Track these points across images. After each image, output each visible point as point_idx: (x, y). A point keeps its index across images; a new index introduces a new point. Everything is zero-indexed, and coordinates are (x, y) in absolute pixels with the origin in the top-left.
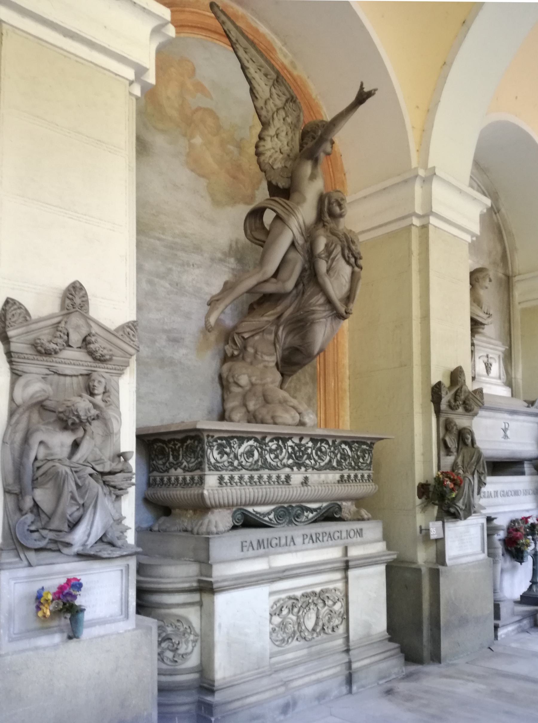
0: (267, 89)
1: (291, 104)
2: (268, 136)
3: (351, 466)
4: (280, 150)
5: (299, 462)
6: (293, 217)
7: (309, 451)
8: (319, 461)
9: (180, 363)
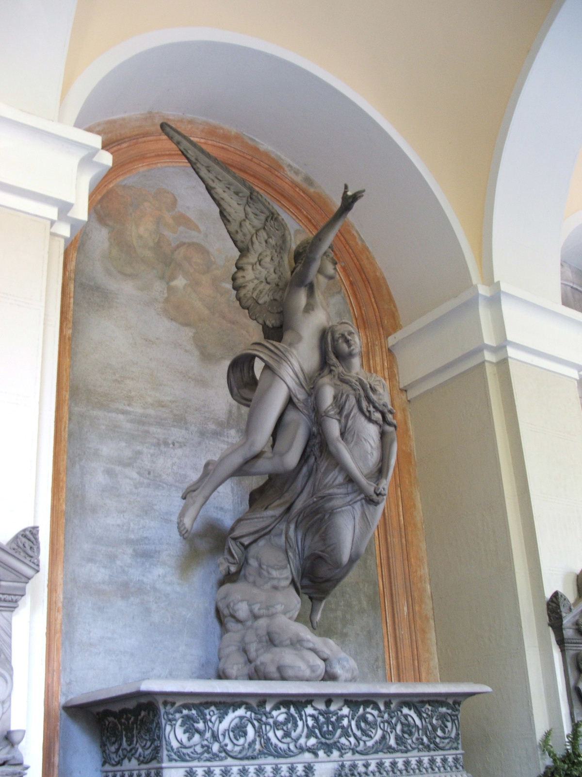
0: (241, 208)
1: (272, 222)
2: (248, 263)
3: (422, 744)
4: (266, 279)
5: (328, 741)
6: (285, 364)
7: (345, 722)
8: (364, 738)
9: (155, 589)
